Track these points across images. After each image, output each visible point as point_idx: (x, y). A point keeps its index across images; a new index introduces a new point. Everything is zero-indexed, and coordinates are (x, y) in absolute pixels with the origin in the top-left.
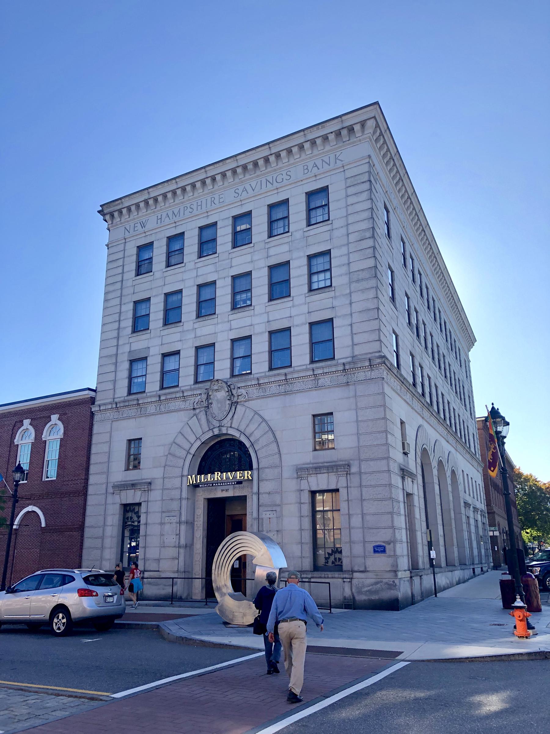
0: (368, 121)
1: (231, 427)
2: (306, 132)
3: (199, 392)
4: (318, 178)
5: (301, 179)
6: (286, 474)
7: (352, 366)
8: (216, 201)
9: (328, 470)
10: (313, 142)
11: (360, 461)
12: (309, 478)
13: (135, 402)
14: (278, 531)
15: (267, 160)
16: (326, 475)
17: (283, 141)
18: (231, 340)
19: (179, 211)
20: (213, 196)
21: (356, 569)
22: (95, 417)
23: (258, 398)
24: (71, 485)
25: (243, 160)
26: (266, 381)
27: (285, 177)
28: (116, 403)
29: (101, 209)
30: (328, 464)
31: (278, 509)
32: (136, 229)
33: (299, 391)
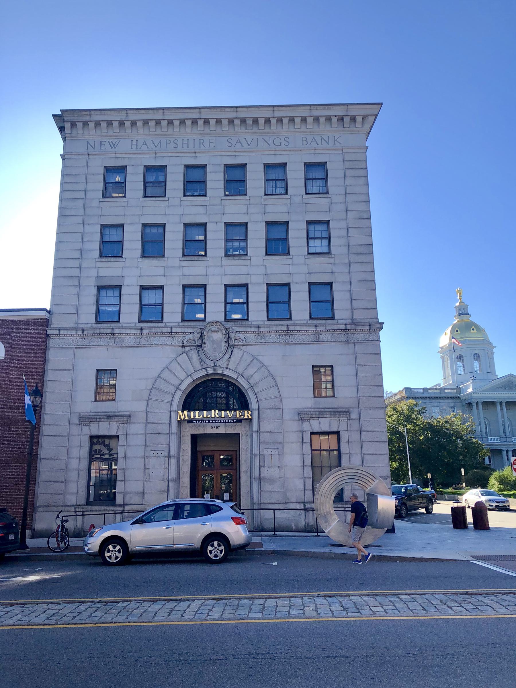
0: (370, 117)
1: (227, 368)
2: (312, 107)
4: (317, 152)
5: (301, 149)
6: (287, 416)
7: (353, 327)
8: (206, 144)
9: (331, 415)
10: (316, 119)
11: (360, 410)
12: (311, 421)
13: (109, 331)
14: (279, 467)
15: (267, 121)
16: (328, 419)
18: (225, 285)
19: (160, 142)
20: (203, 138)
22: (51, 341)
23: (257, 344)
25: (243, 114)
26: (267, 329)
27: (283, 142)
28: (83, 330)
29: (60, 113)
30: (329, 410)
32: (103, 147)
33: (301, 343)
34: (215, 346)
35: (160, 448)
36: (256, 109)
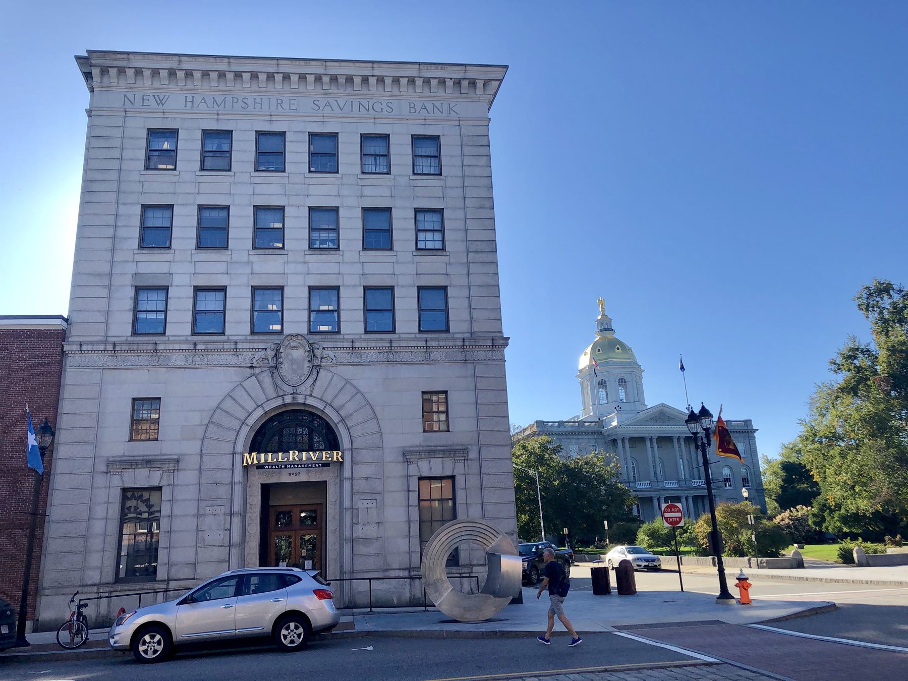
2: (422, 66)
3: (262, 346)
7: (473, 343)
8: (286, 106)
13: (151, 347)
14: (378, 523)
17: (392, 65)
21: (475, 562)
22: (69, 359)
24: (19, 458)
25: (334, 70)
31: (379, 497)
34: (295, 367)
35: (219, 502)
36: (351, 64)
